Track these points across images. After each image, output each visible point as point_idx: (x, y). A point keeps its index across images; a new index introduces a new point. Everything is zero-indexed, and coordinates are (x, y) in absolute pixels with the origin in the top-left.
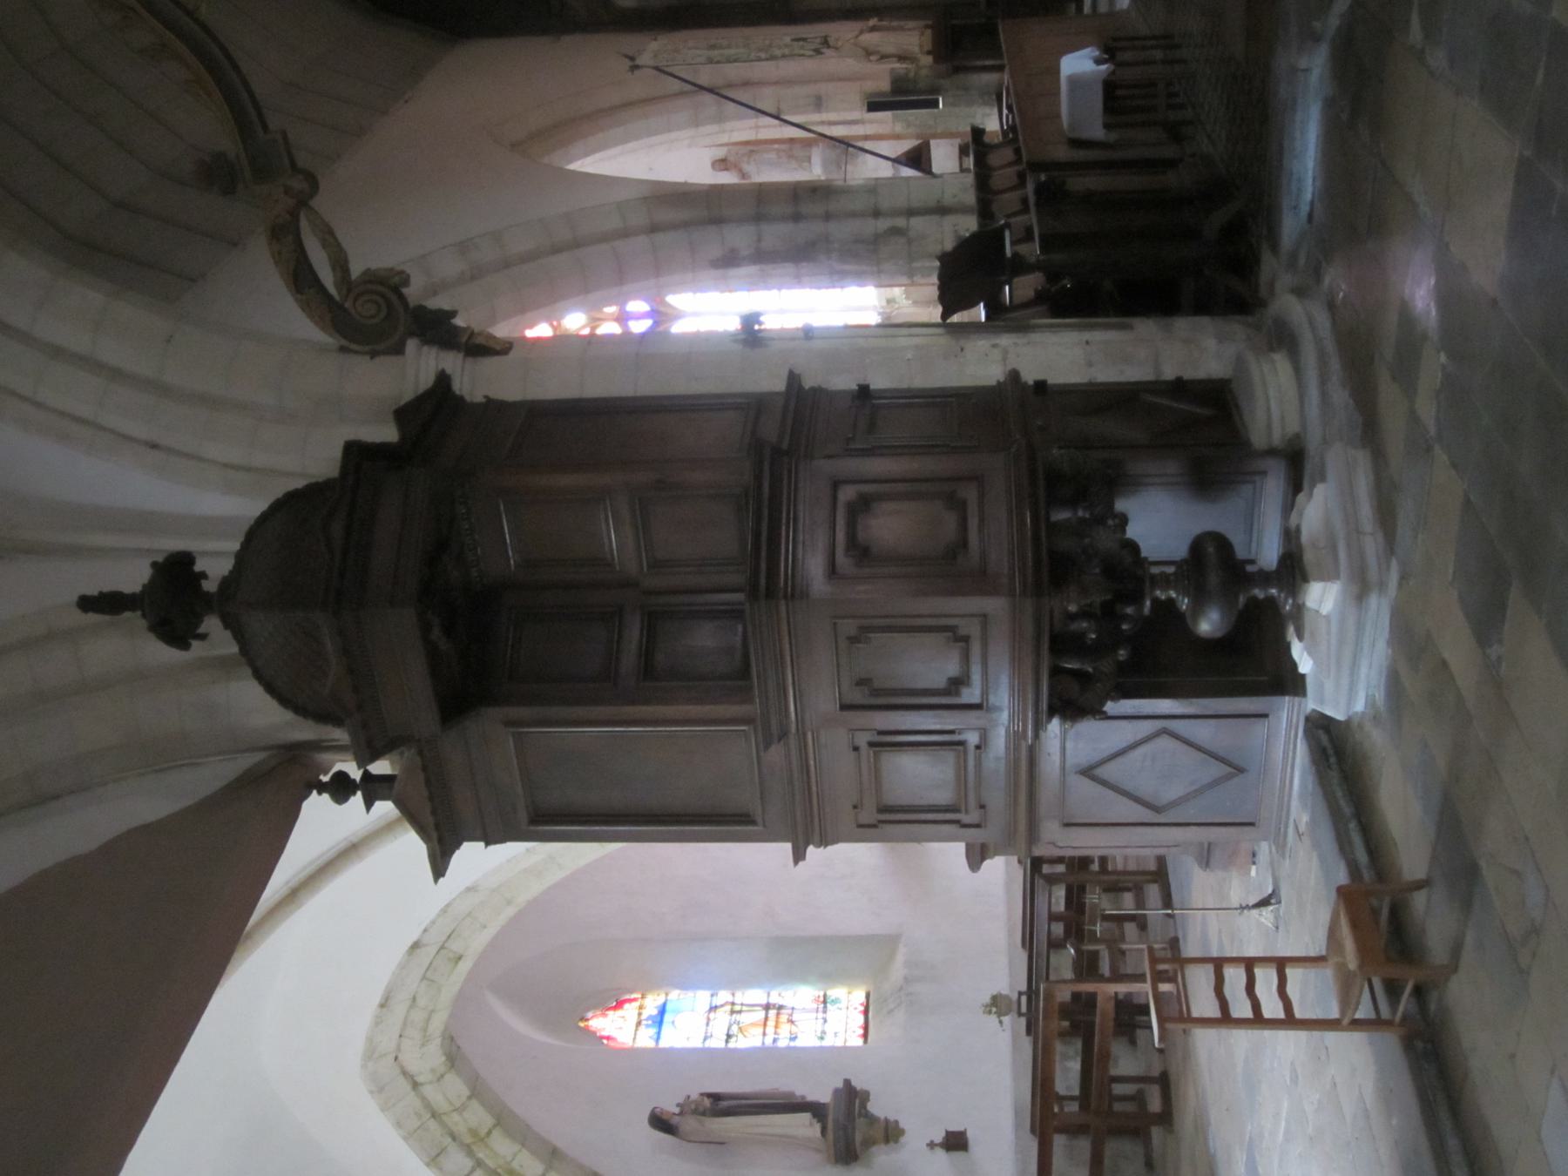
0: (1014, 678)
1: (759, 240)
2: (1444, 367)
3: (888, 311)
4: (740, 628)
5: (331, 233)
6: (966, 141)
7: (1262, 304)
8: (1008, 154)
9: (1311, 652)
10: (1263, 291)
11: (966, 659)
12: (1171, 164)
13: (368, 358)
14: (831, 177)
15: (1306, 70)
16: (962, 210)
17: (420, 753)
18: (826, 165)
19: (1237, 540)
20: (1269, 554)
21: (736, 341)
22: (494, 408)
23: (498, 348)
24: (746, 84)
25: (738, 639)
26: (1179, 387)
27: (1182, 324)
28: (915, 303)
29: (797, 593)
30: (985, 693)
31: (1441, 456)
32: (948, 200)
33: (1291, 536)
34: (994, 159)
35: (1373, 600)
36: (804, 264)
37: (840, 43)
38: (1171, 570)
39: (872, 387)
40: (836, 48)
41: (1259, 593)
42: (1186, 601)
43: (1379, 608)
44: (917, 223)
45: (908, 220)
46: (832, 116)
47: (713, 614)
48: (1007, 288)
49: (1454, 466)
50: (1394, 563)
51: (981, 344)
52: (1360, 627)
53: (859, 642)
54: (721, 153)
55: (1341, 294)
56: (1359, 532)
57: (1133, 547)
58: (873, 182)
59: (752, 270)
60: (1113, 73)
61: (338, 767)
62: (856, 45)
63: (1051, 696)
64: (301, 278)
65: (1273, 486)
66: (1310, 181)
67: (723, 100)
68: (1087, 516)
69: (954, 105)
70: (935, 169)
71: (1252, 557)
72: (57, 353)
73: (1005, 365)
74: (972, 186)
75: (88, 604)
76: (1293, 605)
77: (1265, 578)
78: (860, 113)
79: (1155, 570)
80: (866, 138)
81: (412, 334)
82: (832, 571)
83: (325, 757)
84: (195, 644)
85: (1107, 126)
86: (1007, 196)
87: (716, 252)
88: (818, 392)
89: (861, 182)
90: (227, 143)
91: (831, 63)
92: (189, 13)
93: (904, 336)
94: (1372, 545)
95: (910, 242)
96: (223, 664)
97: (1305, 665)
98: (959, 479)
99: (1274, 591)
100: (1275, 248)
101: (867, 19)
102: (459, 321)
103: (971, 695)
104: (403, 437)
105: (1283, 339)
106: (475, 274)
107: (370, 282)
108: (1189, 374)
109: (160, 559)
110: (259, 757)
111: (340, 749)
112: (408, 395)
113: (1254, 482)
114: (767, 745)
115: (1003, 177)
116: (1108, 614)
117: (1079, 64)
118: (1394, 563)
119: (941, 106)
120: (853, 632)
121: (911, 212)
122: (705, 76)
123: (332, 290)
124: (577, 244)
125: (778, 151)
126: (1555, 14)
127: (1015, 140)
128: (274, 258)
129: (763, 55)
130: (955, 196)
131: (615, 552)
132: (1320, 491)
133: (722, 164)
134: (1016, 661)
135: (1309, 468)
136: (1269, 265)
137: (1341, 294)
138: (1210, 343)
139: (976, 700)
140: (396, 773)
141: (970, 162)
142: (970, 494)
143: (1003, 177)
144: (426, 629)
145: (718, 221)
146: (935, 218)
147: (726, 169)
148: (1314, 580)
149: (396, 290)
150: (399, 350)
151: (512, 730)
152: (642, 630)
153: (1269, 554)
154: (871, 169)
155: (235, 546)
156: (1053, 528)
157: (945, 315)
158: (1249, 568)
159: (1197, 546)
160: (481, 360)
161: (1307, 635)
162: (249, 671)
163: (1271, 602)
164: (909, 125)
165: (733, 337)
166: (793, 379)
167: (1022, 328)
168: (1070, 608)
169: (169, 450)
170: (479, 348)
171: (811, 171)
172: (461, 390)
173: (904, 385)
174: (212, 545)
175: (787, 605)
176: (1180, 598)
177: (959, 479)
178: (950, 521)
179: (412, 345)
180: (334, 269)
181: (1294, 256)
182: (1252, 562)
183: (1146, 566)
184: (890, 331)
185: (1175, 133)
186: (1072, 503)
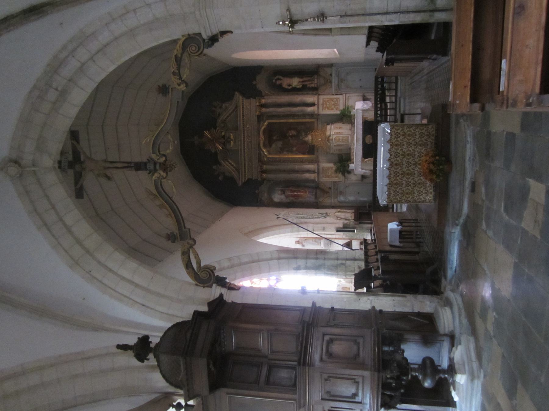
0: (371, 394)
1: (306, 264)
2: (495, 316)
3: (339, 283)
4: (294, 372)
5: (198, 255)
6: (362, 241)
7: (442, 293)
8: (373, 246)
9: (458, 395)
10: (442, 290)
11: (358, 389)
12: (417, 253)
13: (202, 287)
14: (326, 249)
15: (454, 233)
16: (359, 260)
17: (202, 399)
18: (325, 246)
19: (435, 359)
20: (445, 364)
21: (299, 292)
22: (234, 304)
23: (236, 288)
24: (305, 223)
25: (294, 375)
26: (419, 314)
27: (420, 297)
28: (346, 282)
29: (311, 365)
30: (363, 399)
31: (495, 342)
32: (357, 257)
33: (451, 360)
34: (369, 247)
35: (476, 381)
36: (318, 271)
37: (330, 215)
38: (416, 366)
39: (335, 308)
40: (329, 216)
41: (442, 376)
42: (421, 376)
43: (478, 384)
44: (348, 263)
45: (346, 262)
46: (327, 233)
47: (287, 367)
48: (372, 284)
49: (499, 345)
50: (482, 371)
51: (365, 298)
52: (472, 389)
53: (328, 381)
54: (298, 239)
55: (465, 292)
56: (472, 361)
57: (406, 359)
58: (337, 251)
59: (304, 271)
60: (402, 229)
61: (179, 401)
62: (334, 215)
63: (381, 401)
64: (188, 265)
65: (446, 345)
66: (455, 261)
67: (299, 227)
68: (393, 349)
69: (359, 232)
70: (353, 248)
71: (440, 364)
72: (123, 278)
73: (371, 305)
74: (363, 254)
75: (119, 347)
76: (452, 381)
77: (444, 371)
78: (334, 232)
79: (412, 366)
80: (336, 239)
81: (214, 283)
82: (321, 360)
83: (176, 397)
84: (145, 361)
85: (400, 242)
86: (372, 257)
87: (295, 266)
88: (320, 308)
89: (334, 251)
90: (176, 231)
91: (328, 219)
92: (170, 198)
93: (344, 294)
94: (475, 365)
95: (346, 267)
96: (152, 367)
97: (456, 399)
98: (358, 336)
99: (446, 376)
100: (446, 278)
101: (338, 209)
102: (227, 280)
103: (358, 399)
104: (209, 311)
105: (448, 303)
106: (232, 266)
107: (206, 268)
108: (422, 311)
109: (140, 336)
110: (156, 395)
111: (180, 395)
112: (212, 299)
113: (440, 343)
114: (300, 408)
115: (372, 252)
116: (398, 379)
117: (393, 226)
118: (482, 371)
119: (356, 232)
120: (326, 377)
121: (347, 260)
122: (295, 221)
123: (196, 270)
124: (259, 261)
125: (312, 240)
126: (522, 226)
127: (375, 242)
128: (182, 259)
129: (311, 217)
130: (359, 256)
131: (262, 347)
132: (459, 347)
133: (298, 242)
134: (372, 389)
135: (456, 341)
136: (444, 282)
137: (465, 292)
138: (428, 303)
139: (360, 401)
140: (194, 404)
141: (363, 247)
142: (361, 341)
143: (372, 252)
144: (208, 365)
145: (296, 258)
146: (353, 261)
147: (299, 244)
148: (459, 374)
149: (212, 271)
150: (211, 286)
151: (228, 395)
152: (267, 370)
153: (445, 364)
154: (336, 247)
155: (161, 334)
156: (384, 352)
157: (355, 290)
158: (439, 368)
159: (424, 360)
160: (231, 291)
161: (456, 389)
162: (159, 371)
163: (446, 379)
164: (347, 236)
165: (299, 291)
166: (314, 304)
167: (376, 295)
168: (388, 376)
169: (148, 307)
170: (232, 288)
171: (320, 246)
172: (226, 298)
173: (343, 308)
174: (154, 334)
175: (308, 368)
176: (419, 375)
177: (358, 336)
178: (355, 348)
179: (214, 285)
180: (197, 264)
181: (451, 281)
182: (440, 366)
183: (409, 365)
184: (340, 293)
185: (418, 244)
186: (389, 345)
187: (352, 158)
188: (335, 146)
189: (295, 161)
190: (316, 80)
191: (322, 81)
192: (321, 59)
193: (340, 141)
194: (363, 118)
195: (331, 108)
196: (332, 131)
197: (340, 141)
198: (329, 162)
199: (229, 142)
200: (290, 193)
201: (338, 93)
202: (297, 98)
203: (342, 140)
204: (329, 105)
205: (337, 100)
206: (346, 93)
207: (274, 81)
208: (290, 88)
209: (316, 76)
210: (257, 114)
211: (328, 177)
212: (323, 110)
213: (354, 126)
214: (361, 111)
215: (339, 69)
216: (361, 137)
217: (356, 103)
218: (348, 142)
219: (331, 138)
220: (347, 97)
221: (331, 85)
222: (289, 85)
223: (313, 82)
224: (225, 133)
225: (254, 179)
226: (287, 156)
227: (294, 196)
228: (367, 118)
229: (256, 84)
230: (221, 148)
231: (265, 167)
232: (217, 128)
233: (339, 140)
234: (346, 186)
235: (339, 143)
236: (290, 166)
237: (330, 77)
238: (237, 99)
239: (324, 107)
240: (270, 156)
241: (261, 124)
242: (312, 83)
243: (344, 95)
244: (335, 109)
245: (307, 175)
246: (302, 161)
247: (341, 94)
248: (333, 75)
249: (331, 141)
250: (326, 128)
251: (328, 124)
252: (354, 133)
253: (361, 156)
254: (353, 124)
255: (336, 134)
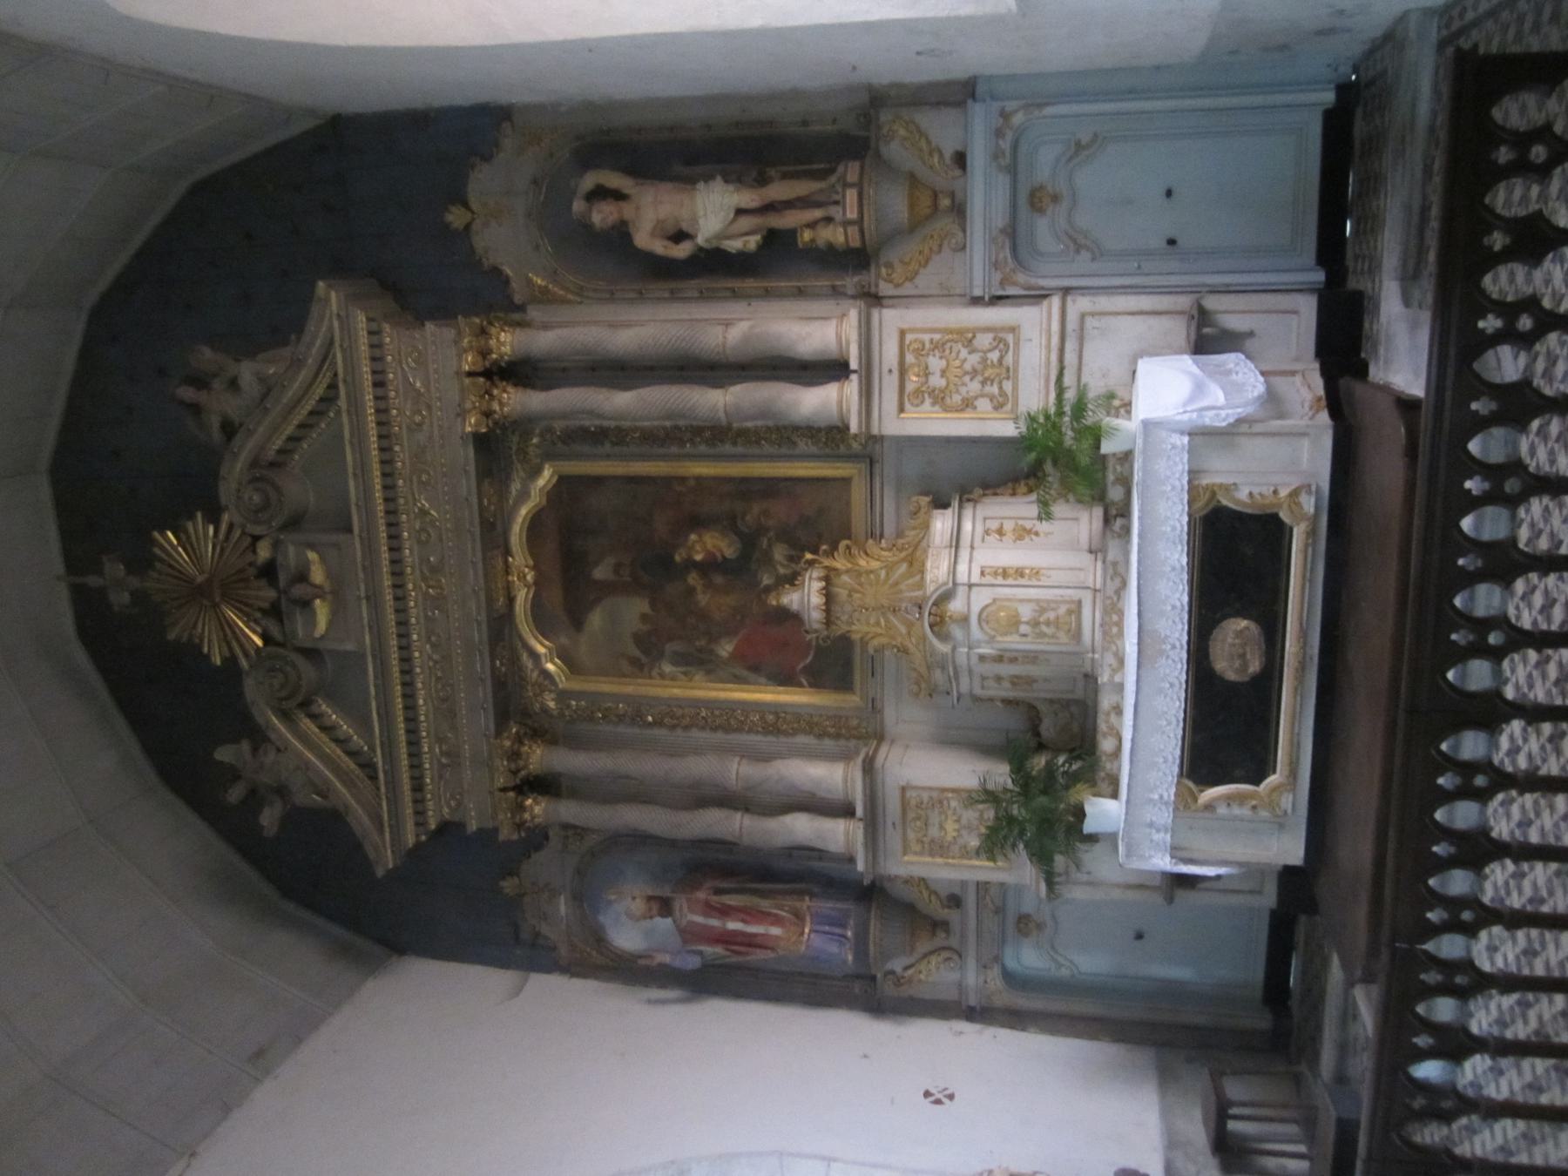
58: (1034, 859)
187: (1106, 745)
188: (982, 658)
189: (729, 719)
190: (851, 196)
191: (895, 204)
192: (868, 27)
193: (1024, 629)
194: (1193, 489)
195: (957, 399)
196: (964, 554)
197: (1024, 629)
198: (952, 739)
199: (306, 604)
200: (699, 919)
201: (1011, 291)
202: (728, 324)
203: (1035, 623)
204: (943, 373)
205: (1000, 343)
206: (1066, 291)
207: (578, 206)
208: (682, 251)
209: (852, 171)
210: (469, 429)
211: (938, 848)
212: (901, 409)
213: (1127, 530)
214: (1186, 439)
215: (1018, 119)
216: (1175, 629)
217: (1143, 365)
218: (1077, 635)
219: (956, 606)
220: (1072, 324)
221: (964, 231)
222: (679, 236)
223: (835, 212)
224: (276, 545)
225: (473, 826)
226: (677, 692)
227: (727, 939)
228: (1227, 489)
229: (468, 227)
230: (259, 642)
231: (538, 758)
232: (226, 517)
233: (1014, 622)
234: (1079, 147)
235: (1012, 642)
236: (701, 767)
237: (958, 172)
238: (331, 328)
239: (910, 387)
240: (577, 685)
241: (515, 487)
242: (829, 220)
243: (1056, 301)
244: (984, 405)
245: (802, 828)
246: (777, 723)
247: (1037, 297)
248: (978, 159)
249: (957, 632)
250: (926, 526)
251: (941, 504)
252: (1124, 584)
253: (1176, 770)
254: (1116, 516)
255: (988, 579)
